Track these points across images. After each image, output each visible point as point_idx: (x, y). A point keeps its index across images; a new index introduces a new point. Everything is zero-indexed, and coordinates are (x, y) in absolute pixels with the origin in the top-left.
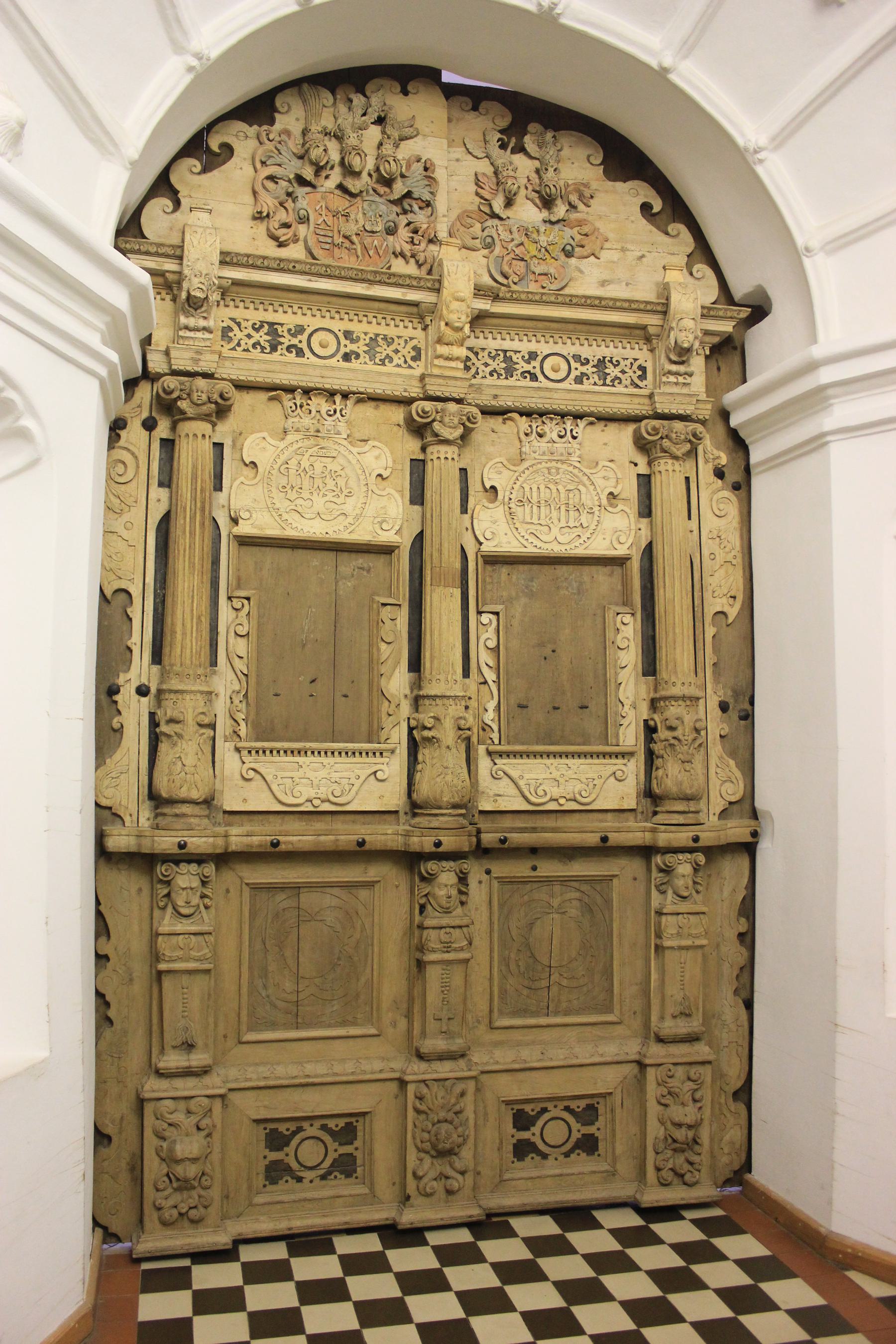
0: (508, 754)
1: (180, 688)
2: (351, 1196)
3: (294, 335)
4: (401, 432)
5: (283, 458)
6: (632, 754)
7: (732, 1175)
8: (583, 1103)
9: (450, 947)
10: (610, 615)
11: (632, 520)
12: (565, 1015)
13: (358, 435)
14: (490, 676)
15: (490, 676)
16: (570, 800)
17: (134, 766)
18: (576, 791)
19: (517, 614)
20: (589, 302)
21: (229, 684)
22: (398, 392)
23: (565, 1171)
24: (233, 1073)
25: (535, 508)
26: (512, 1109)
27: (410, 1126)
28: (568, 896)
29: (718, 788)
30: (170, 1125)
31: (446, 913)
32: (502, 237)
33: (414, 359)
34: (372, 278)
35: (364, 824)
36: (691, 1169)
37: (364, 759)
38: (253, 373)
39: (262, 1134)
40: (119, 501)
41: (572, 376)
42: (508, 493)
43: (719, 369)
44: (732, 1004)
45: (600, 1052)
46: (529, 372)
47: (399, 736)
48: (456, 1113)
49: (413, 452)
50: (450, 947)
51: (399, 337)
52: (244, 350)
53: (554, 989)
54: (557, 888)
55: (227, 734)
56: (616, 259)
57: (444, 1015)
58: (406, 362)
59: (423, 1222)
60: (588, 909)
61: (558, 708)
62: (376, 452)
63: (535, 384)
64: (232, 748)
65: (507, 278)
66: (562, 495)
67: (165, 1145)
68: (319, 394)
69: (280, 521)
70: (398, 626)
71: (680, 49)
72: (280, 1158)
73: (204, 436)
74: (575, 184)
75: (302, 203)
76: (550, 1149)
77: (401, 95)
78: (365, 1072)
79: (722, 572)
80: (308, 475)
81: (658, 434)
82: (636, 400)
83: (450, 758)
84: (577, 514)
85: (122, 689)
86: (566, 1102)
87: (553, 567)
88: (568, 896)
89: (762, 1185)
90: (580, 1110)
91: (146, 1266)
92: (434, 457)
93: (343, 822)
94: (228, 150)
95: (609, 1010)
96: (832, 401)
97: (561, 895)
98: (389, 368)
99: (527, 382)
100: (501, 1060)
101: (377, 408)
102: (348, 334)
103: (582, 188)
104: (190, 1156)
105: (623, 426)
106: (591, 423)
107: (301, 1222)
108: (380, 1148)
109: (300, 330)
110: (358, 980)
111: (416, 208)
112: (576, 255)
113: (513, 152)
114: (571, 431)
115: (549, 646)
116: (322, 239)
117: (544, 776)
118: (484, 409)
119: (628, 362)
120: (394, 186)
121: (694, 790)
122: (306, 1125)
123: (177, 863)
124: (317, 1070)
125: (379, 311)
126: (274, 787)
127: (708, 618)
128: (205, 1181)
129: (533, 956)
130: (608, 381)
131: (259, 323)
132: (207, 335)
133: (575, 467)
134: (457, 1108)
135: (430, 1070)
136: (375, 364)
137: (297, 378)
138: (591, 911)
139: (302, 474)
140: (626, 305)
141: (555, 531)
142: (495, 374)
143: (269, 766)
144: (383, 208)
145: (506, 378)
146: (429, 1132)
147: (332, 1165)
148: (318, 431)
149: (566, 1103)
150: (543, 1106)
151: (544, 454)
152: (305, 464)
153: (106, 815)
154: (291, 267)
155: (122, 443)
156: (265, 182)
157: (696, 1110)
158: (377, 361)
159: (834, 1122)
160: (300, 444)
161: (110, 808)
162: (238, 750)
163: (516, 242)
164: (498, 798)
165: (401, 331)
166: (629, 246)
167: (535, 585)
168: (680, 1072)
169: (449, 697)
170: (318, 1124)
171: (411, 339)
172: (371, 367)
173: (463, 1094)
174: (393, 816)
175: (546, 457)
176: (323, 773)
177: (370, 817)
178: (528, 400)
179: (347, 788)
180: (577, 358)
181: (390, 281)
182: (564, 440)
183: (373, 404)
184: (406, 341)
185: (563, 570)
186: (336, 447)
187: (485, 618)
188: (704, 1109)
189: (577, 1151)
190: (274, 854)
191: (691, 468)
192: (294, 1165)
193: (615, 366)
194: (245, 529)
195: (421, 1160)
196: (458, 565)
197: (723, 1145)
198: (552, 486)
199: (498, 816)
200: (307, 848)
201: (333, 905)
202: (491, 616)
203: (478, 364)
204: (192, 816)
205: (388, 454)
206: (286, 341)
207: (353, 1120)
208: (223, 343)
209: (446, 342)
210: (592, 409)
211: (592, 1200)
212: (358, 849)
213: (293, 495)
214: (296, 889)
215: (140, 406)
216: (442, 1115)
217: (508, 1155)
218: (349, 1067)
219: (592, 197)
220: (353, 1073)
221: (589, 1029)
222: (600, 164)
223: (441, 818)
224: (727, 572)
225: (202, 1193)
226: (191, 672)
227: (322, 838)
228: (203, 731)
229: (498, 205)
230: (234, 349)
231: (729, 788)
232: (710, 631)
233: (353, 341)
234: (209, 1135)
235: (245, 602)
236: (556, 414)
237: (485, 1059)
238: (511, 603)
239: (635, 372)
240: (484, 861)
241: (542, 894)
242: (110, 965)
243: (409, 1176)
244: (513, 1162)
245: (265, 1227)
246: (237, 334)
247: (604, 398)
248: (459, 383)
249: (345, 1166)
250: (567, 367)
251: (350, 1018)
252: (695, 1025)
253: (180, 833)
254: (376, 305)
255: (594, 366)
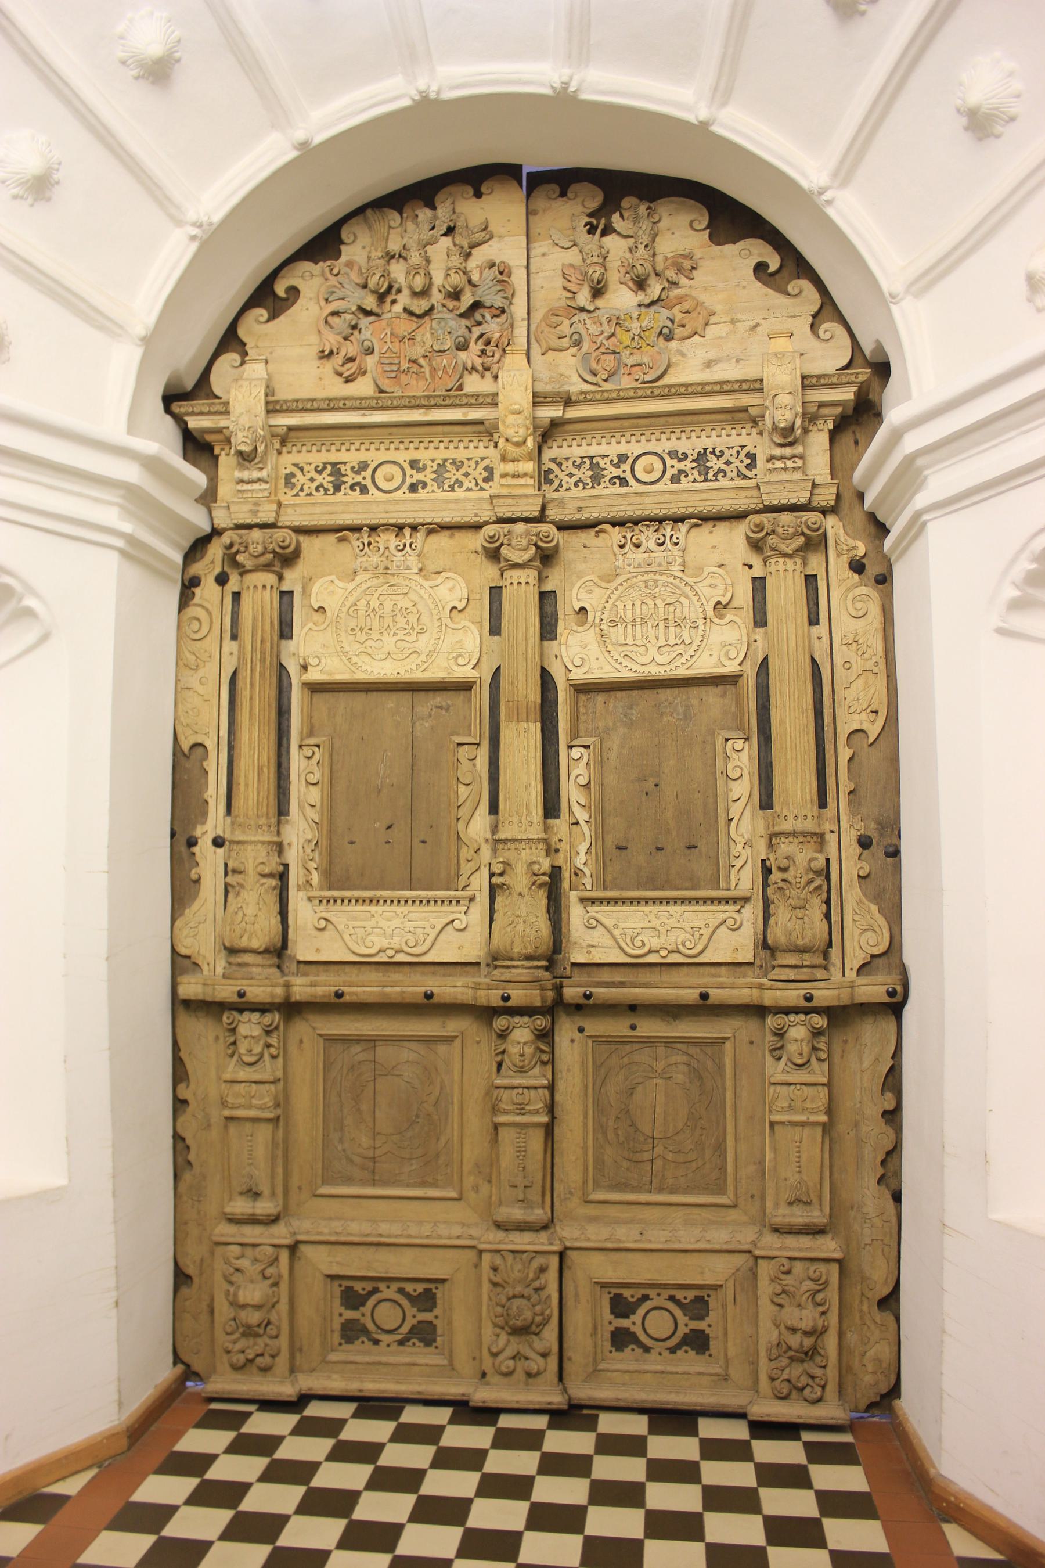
0: (601, 901)
1: (241, 838)
2: (427, 1365)
3: (358, 473)
4: (479, 560)
5: (352, 600)
6: (746, 900)
7: (878, 1399)
8: (691, 1294)
9: (523, 1109)
10: (719, 742)
11: (744, 631)
12: (671, 1193)
13: (432, 567)
14: (582, 815)
15: (582, 815)
16: (673, 952)
17: (211, 916)
18: (679, 941)
19: (615, 747)
20: (673, 391)
21: (301, 832)
22: (469, 518)
23: (669, 1369)
24: (306, 1225)
25: (629, 627)
26: (609, 1293)
27: (485, 1298)
28: (674, 1059)
29: (856, 938)
30: (237, 1270)
31: (521, 1072)
32: (590, 332)
33: (486, 480)
34: (426, 403)
35: (444, 976)
36: (811, 1382)
37: (439, 907)
38: (316, 517)
39: (337, 1291)
40: (194, 658)
41: (668, 475)
42: (598, 614)
43: (856, 443)
44: (876, 1195)
45: (708, 1238)
46: (618, 477)
47: (480, 883)
48: (536, 1290)
49: (493, 580)
50: (523, 1109)
51: (469, 459)
52: (307, 495)
53: (658, 1163)
54: (661, 1050)
55: (300, 883)
56: (724, 334)
57: (519, 1181)
58: (477, 484)
59: (496, 1402)
60: (696, 1074)
61: (662, 849)
62: (450, 583)
63: (624, 490)
64: (305, 898)
65: (596, 375)
66: (661, 610)
67: (232, 1289)
68: (387, 529)
69: (349, 665)
70: (478, 766)
71: (713, 98)
72: (349, 1312)
73: (264, 586)
74: (673, 257)
75: (366, 334)
76: (653, 1342)
77: (474, 199)
78: (440, 1237)
79: (860, 682)
80: (378, 615)
81: (762, 530)
82: (743, 493)
83: (523, 906)
84: (678, 629)
85: (199, 841)
86: (673, 1294)
87: (655, 691)
88: (674, 1059)
89: (905, 1414)
90: (687, 1301)
91: (214, 1406)
92: (507, 583)
93: (423, 974)
94: (294, 292)
95: (721, 1190)
96: (926, 473)
97: (666, 1057)
98: (459, 494)
99: (617, 489)
100: (593, 1237)
101: (452, 536)
102: (414, 464)
103: (680, 260)
104: (252, 1303)
105: (735, 523)
106: (696, 525)
107: (372, 1386)
108: (463, 1317)
109: (364, 466)
110: (438, 1139)
111: (488, 317)
112: (675, 337)
113: (604, 233)
114: (672, 536)
115: (651, 779)
116: (387, 368)
117: (642, 925)
118: (561, 524)
119: (734, 452)
120: (462, 299)
121: (807, 940)
122: (382, 1286)
123: (241, 1011)
124: (390, 1230)
125: (445, 435)
126: (346, 937)
127: (842, 739)
128: (272, 1330)
129: (633, 1124)
130: (710, 476)
131: (321, 465)
132: (264, 486)
133: (676, 577)
134: (537, 1284)
135: (507, 1240)
136: (444, 491)
137: (360, 516)
138: (700, 1077)
139: (372, 615)
140: (717, 388)
141: (653, 651)
142: (581, 485)
143: (339, 915)
144: (452, 323)
145: (593, 487)
146: (503, 1306)
147: (411, 1331)
148: (387, 568)
149: (672, 1292)
150: (646, 1292)
151: (639, 566)
152: (374, 603)
153: (181, 963)
154: (341, 405)
155: (196, 600)
156: (330, 319)
157: (817, 1316)
158: (446, 487)
159: (942, 1341)
160: (369, 584)
161: (189, 957)
162: (310, 899)
163: (606, 334)
164: (592, 949)
165: (472, 452)
166: (739, 316)
167: (635, 714)
168: (798, 1267)
169: (521, 841)
170: (395, 1286)
171: (483, 459)
172: (440, 495)
173: (543, 1270)
174: (476, 968)
175: (642, 570)
176: (396, 923)
177: (451, 968)
178: (616, 509)
179: (422, 938)
180: (673, 454)
181: (446, 403)
182: (662, 548)
183: (447, 533)
184: (477, 463)
185: (666, 694)
186: (407, 582)
187: (576, 753)
188: (829, 1314)
189: (685, 1348)
190: (337, 1005)
191: (819, 564)
192: (371, 1326)
193: (718, 457)
194: (314, 675)
195: (498, 1336)
196: (534, 696)
197: (865, 1361)
198: (649, 601)
199: (595, 968)
200: (371, 999)
201: (410, 1059)
202: (582, 750)
203: (562, 475)
204: (253, 965)
205: (463, 585)
206: (349, 480)
207: (432, 1286)
208: (286, 490)
209: (510, 458)
210: (691, 510)
211: (696, 1404)
212: (426, 1001)
213: (362, 637)
214: (371, 1041)
215: (213, 562)
216: (519, 1289)
217: (605, 1343)
218: (426, 1230)
219: (693, 268)
220: (428, 1237)
221: (696, 1210)
222: (705, 229)
223: (514, 971)
224: (866, 683)
225: (268, 1341)
226: (252, 823)
227: (388, 989)
228: (264, 880)
229: (583, 298)
230: (297, 495)
231: (870, 937)
232: (845, 753)
233: (419, 470)
234: (276, 1284)
235: (317, 749)
236: (652, 520)
237: (577, 1233)
238: (608, 734)
239: (742, 461)
240: (577, 1018)
241: (643, 1056)
242: (190, 1110)
243: (485, 1352)
244: (611, 1352)
245: (336, 1384)
246: (300, 479)
247: (704, 496)
248: (531, 501)
249: (425, 1334)
250: (661, 466)
251: (430, 1180)
252: (817, 1216)
253: (239, 982)
254: (440, 429)
255: (693, 461)
